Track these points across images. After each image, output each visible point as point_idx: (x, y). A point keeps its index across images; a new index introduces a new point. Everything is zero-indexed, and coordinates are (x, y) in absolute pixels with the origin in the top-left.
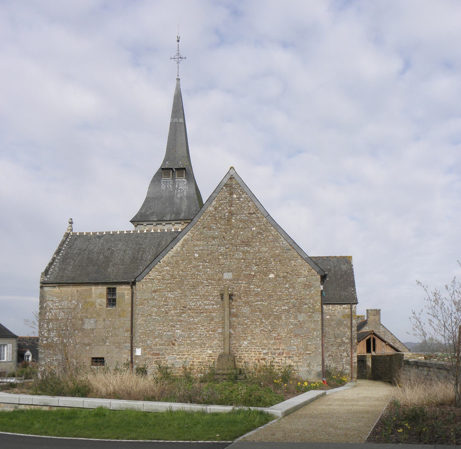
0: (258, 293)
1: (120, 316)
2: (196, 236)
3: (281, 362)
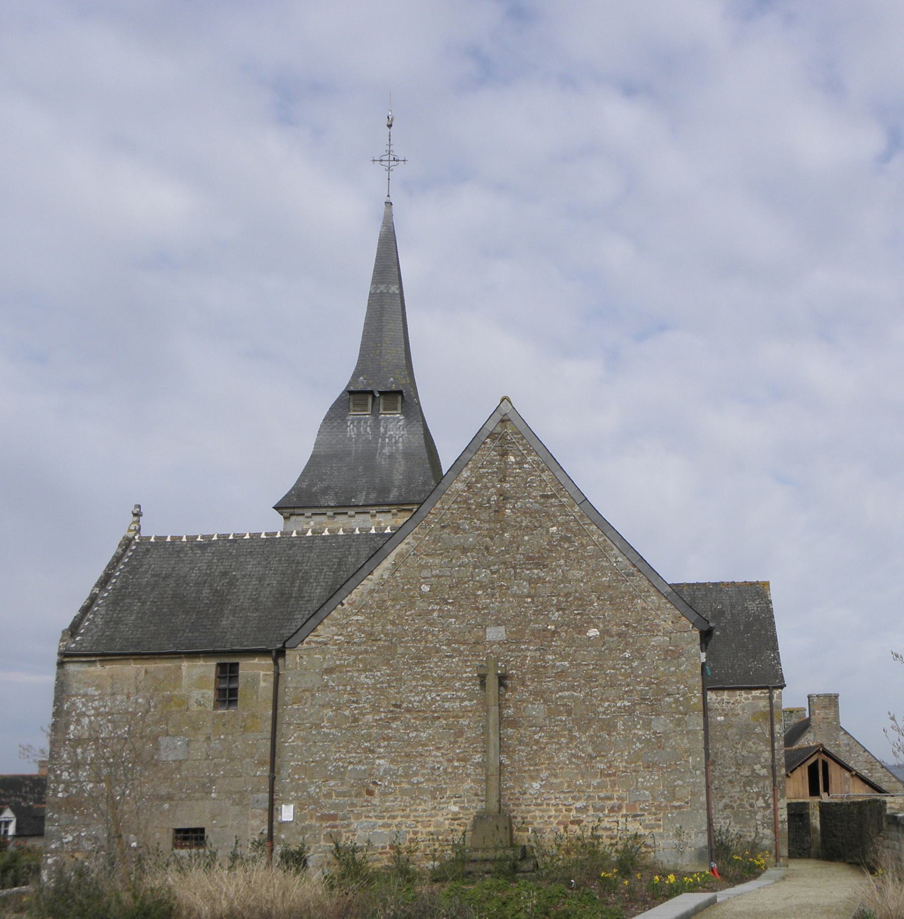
0: (562, 671)
1: (245, 729)
2: (426, 545)
3: (616, 828)
